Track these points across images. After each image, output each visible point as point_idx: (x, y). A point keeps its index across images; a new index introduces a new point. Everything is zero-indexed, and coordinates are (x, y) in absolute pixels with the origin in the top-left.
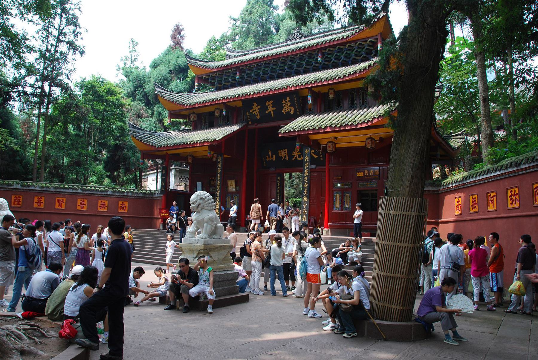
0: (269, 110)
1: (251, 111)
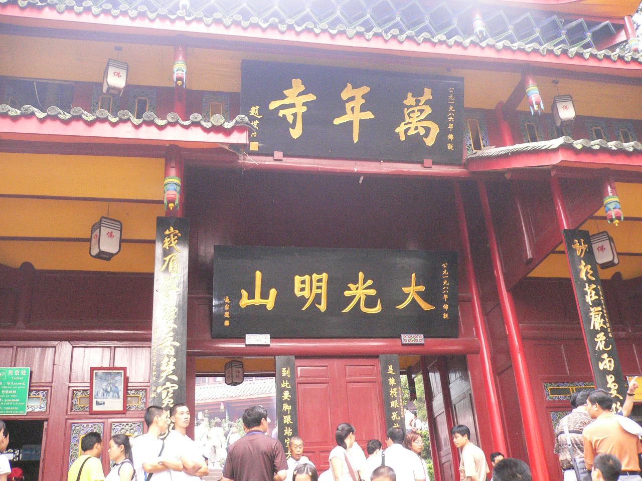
1: (273, 105)
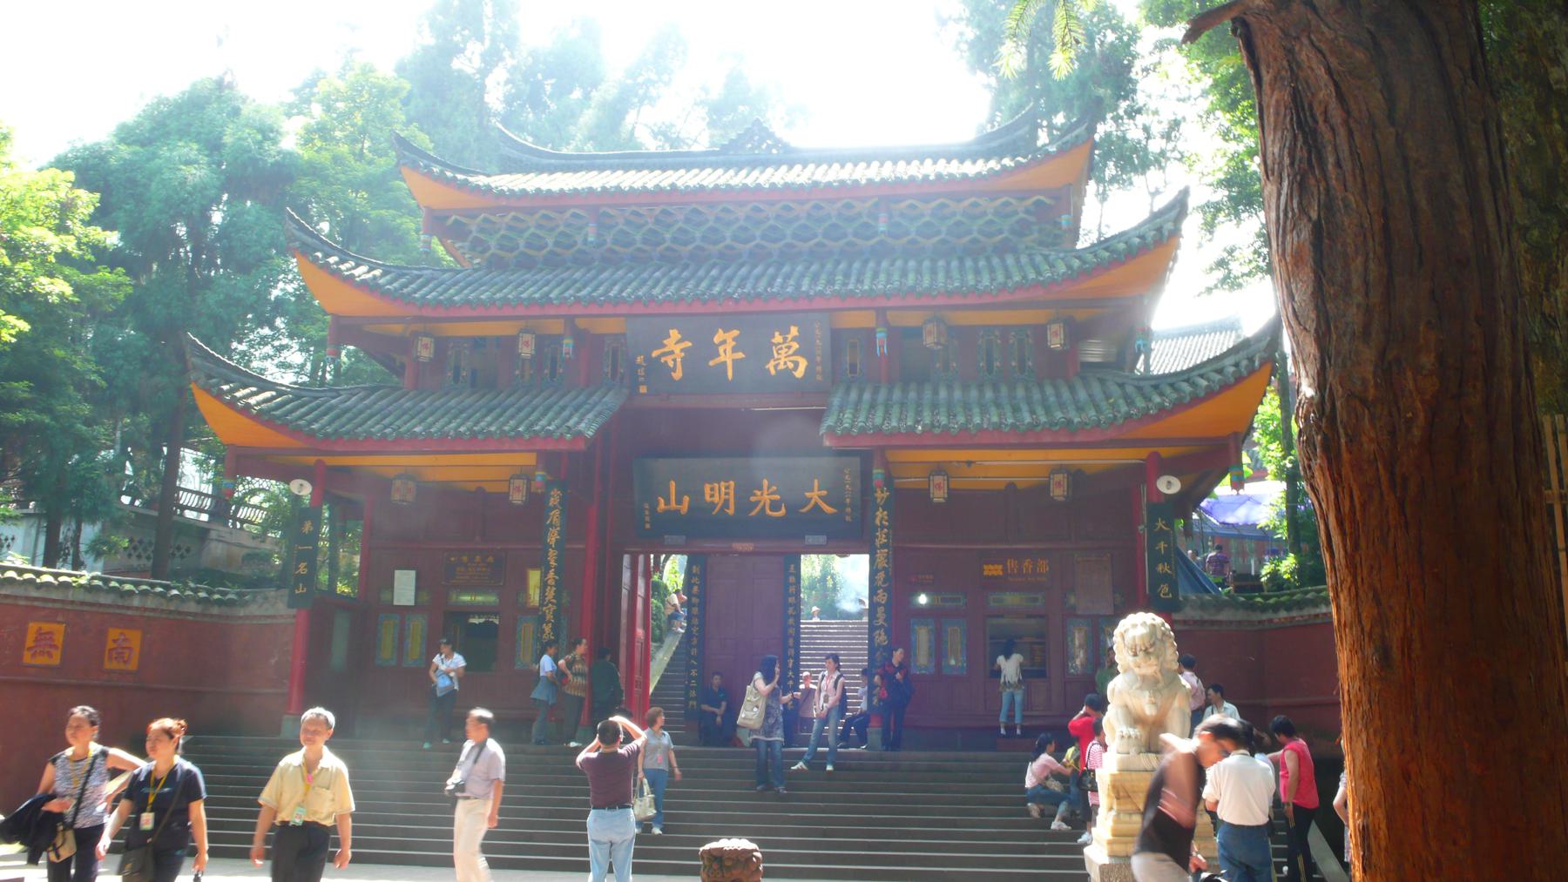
0: (722, 358)
1: (655, 354)
